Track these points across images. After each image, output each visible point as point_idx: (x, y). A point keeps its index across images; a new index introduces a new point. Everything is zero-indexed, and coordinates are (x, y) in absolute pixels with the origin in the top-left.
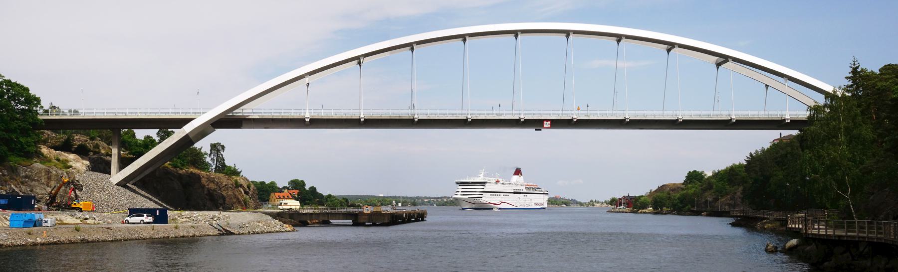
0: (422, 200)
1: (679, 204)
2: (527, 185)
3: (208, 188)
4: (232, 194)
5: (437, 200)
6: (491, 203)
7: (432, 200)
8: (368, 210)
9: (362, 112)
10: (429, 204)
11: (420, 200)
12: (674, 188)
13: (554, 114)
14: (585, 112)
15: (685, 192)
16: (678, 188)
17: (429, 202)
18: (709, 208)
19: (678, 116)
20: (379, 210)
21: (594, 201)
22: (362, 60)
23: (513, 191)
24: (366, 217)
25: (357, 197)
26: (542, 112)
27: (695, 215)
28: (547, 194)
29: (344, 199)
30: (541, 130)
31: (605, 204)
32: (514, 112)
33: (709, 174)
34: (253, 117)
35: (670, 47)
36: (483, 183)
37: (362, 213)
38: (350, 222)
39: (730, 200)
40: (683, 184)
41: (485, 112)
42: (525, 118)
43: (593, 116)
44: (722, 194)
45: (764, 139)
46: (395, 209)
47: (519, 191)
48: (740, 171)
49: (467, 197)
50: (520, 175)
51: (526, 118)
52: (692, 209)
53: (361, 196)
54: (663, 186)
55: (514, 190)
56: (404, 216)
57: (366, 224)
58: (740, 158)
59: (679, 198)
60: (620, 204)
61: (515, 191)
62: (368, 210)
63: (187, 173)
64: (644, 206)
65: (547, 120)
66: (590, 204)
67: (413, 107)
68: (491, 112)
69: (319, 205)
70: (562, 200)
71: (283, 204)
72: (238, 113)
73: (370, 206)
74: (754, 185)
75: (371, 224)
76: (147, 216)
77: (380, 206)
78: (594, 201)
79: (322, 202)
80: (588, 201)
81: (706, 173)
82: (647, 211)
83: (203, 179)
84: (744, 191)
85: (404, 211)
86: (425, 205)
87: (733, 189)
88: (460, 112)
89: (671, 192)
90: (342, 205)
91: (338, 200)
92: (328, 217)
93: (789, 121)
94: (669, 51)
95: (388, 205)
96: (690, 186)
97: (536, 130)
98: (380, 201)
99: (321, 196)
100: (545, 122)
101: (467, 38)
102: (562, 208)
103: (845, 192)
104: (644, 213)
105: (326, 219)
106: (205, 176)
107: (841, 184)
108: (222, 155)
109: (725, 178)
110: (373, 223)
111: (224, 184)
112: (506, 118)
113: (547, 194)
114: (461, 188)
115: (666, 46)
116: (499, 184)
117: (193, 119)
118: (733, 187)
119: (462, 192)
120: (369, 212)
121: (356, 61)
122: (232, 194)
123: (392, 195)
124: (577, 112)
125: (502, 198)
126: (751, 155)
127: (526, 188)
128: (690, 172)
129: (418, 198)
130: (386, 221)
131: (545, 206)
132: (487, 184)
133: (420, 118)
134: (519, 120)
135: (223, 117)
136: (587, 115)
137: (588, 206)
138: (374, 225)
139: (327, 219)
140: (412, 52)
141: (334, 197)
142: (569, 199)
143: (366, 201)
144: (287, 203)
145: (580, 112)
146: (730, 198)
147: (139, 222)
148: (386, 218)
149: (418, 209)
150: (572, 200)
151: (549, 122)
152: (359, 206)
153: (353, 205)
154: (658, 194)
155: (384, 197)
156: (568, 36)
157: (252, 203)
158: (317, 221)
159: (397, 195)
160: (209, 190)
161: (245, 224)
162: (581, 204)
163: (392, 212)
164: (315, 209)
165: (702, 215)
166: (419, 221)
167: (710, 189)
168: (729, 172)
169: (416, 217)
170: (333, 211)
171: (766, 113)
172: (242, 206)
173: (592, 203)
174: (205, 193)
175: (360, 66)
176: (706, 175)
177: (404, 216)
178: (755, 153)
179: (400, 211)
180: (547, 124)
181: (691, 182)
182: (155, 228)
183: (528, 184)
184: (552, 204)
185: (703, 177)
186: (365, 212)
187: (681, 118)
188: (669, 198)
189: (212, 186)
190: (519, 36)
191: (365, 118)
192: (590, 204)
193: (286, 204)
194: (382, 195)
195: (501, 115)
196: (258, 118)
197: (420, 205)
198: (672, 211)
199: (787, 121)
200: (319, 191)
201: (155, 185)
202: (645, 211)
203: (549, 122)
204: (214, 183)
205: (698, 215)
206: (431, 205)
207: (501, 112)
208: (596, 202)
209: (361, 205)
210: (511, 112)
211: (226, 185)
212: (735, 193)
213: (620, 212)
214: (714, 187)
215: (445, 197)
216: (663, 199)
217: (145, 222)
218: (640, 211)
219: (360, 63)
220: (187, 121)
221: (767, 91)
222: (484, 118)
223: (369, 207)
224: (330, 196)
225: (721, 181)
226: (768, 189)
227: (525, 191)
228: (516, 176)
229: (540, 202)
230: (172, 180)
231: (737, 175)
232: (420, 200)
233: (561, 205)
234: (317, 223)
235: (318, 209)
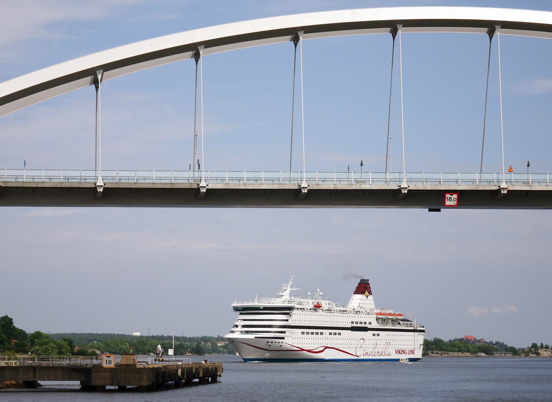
0: (214, 344)
2: (380, 314)
6: (303, 350)
8: (110, 362)
9: (100, 174)
10: (225, 350)
11: (210, 344)
13: (464, 181)
14: (524, 177)
17: (225, 347)
20: (131, 362)
21: (539, 345)
22: (99, 77)
23: (350, 326)
24: (107, 375)
25: (91, 338)
26: (442, 176)
28: (423, 331)
29: (65, 340)
30: (439, 210)
32: (389, 176)
36: (287, 310)
37: (99, 367)
38: (76, 384)
41: (335, 175)
42: (410, 188)
43: (537, 184)
46: (163, 360)
47: (363, 325)
49: (252, 336)
50: (367, 293)
51: (412, 187)
53: (99, 335)
55: (352, 323)
56: (179, 373)
57: (107, 387)
61: (355, 325)
62: (110, 362)
65: (452, 192)
66: (530, 351)
67: (197, 166)
68: (345, 175)
69: (17, 351)
70: (479, 344)
73: (115, 353)
75: (117, 387)
77: (133, 354)
79: (23, 345)
80: (527, 345)
85: (180, 363)
86: (219, 352)
88: (287, 175)
90: (60, 353)
91: (54, 343)
95: (149, 351)
97: (429, 211)
98: (134, 345)
99: (21, 334)
100: (448, 196)
101: (202, 51)
102: (478, 360)
105: (31, 378)
110: (119, 387)
112: (374, 187)
113: (423, 331)
114: (241, 320)
116: (320, 312)
119: (244, 326)
120: (112, 365)
121: (89, 79)
123: (155, 335)
124: (508, 176)
125: (326, 338)
127: (377, 319)
129: (205, 339)
130: (145, 383)
131: (418, 354)
132: (295, 312)
134: (399, 191)
136: (527, 183)
137: (527, 355)
138: (122, 389)
139: (32, 379)
140: (197, 61)
141: (47, 336)
142: (491, 343)
143: (108, 345)
145: (513, 176)
148: (145, 377)
149: (206, 361)
150: (497, 343)
151: (455, 196)
152: (93, 355)
153: (81, 353)
155: (142, 337)
156: (491, 33)
158: (13, 382)
159: (166, 334)
162: (514, 351)
163: (156, 366)
164: (9, 359)
166: (207, 383)
169: (201, 375)
170: (44, 363)
173: (535, 349)
175: (97, 88)
177: (179, 373)
179: (171, 363)
180: (450, 199)
183: (383, 312)
184: (459, 351)
186: (105, 365)
190: (400, 32)
191: (106, 186)
194: (138, 334)
195: (364, 182)
197: (209, 353)
200: (18, 324)
206: (229, 353)
207: (364, 176)
208: (542, 346)
209: (98, 352)
210: (383, 176)
219: (96, 82)
222: (332, 187)
223: (112, 358)
224: (38, 335)
227: (375, 325)
228: (359, 296)
229: (408, 347)
232: (210, 344)
233: (477, 352)
234: (14, 386)
235: (16, 359)
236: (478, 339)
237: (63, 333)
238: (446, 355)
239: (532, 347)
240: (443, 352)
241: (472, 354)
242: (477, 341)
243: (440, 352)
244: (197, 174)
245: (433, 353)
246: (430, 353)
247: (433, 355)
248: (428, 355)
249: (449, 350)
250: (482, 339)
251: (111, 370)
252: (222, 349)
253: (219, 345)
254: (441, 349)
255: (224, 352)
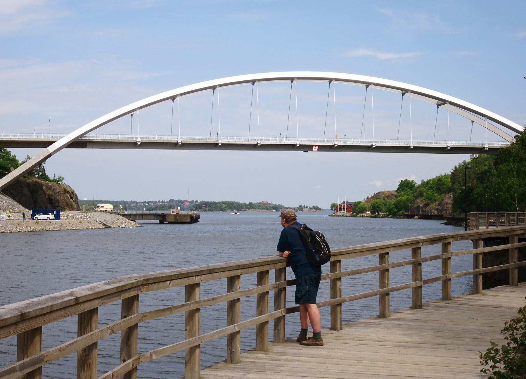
0: (129, 205)
1: (394, 209)
3: (48, 194)
4: (63, 198)
5: (144, 205)
7: (138, 204)
10: (135, 208)
12: (389, 195)
15: (399, 198)
16: (392, 195)
17: (135, 206)
18: (421, 213)
19: (410, 144)
21: (303, 206)
27: (408, 218)
30: (308, 152)
31: (314, 209)
33: (418, 182)
34: (97, 141)
35: (404, 92)
38: (157, 221)
39: (438, 206)
40: (396, 191)
41: (19, 135)
44: (431, 201)
45: (467, 158)
48: (446, 181)
52: (406, 213)
54: (379, 193)
58: (448, 170)
59: (394, 204)
60: (341, 209)
62: (174, 212)
63: (33, 182)
64: (363, 210)
65: (316, 146)
66: (298, 209)
71: (100, 207)
72: (86, 137)
74: (461, 194)
76: (52, 214)
78: (303, 206)
81: (415, 182)
82: (365, 215)
83: (43, 187)
84: (454, 199)
87: (441, 196)
89: (386, 199)
92: (143, 216)
93: (487, 149)
94: (403, 94)
96: (403, 193)
97: (304, 152)
100: (314, 147)
103: (515, 201)
104: (363, 216)
106: (45, 185)
107: (513, 198)
108: (43, 167)
109: (434, 187)
110: (168, 222)
111: (58, 190)
115: (402, 91)
117: (54, 142)
118: (440, 195)
120: (175, 214)
122: (63, 198)
123: (97, 200)
126: (456, 168)
128: (402, 181)
133: (223, 143)
135: (76, 140)
144: (103, 206)
146: (439, 204)
147: (46, 218)
151: (317, 147)
154: (376, 200)
157: (235, 203)
160: (48, 195)
161: (115, 221)
165: (415, 219)
167: (421, 197)
168: (438, 182)
171: (472, 142)
172: (70, 208)
174: (46, 197)
176: (416, 184)
178: (458, 166)
181: (403, 189)
182: (71, 222)
184: (263, 209)
185: (414, 186)
186: (172, 213)
187: (412, 145)
188: (385, 204)
189: (49, 192)
192: (298, 209)
193: (102, 207)
194: (86, 199)
196: (101, 141)
198: (388, 215)
199: (486, 149)
201: (12, 191)
202: (363, 215)
203: (317, 147)
204: (51, 190)
205: (411, 218)
208: (304, 207)
211: (59, 192)
212: (443, 200)
213: (341, 216)
214: (425, 194)
215: (152, 202)
216: (380, 205)
217: (51, 218)
218: (359, 215)
220: (50, 143)
221: (472, 125)
225: (430, 189)
226: (472, 198)
230: (23, 187)
231: (444, 184)
233: (271, 210)
236: (269, 203)
237: (79, 198)
238: (255, 211)
239: (299, 207)
240: (254, 209)
241: (269, 210)
242: (269, 204)
243: (252, 210)
244: (216, 138)
245: (249, 210)
246: (247, 210)
247: (249, 211)
248: (246, 211)
249: (257, 208)
250: (271, 203)
251: (174, 215)
252: (134, 207)
253: (132, 205)
254: (253, 208)
255: (135, 209)
